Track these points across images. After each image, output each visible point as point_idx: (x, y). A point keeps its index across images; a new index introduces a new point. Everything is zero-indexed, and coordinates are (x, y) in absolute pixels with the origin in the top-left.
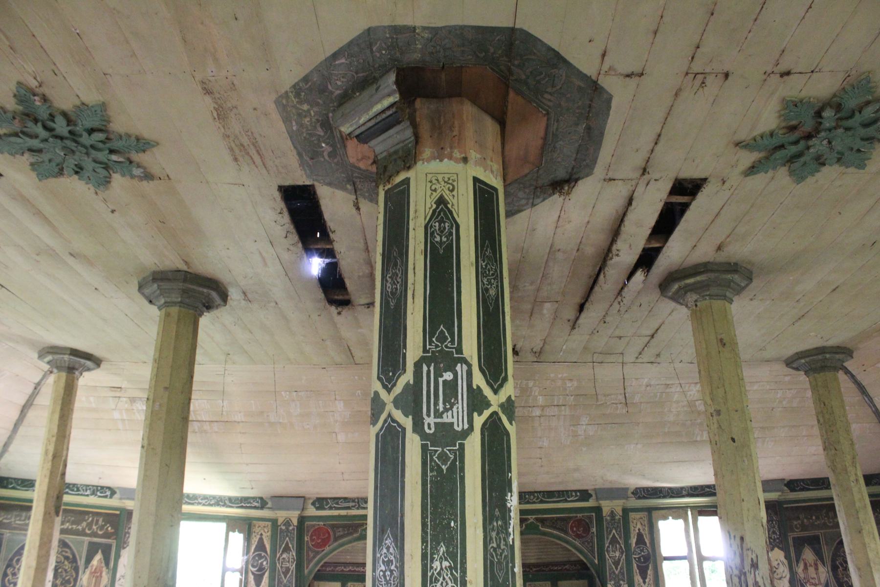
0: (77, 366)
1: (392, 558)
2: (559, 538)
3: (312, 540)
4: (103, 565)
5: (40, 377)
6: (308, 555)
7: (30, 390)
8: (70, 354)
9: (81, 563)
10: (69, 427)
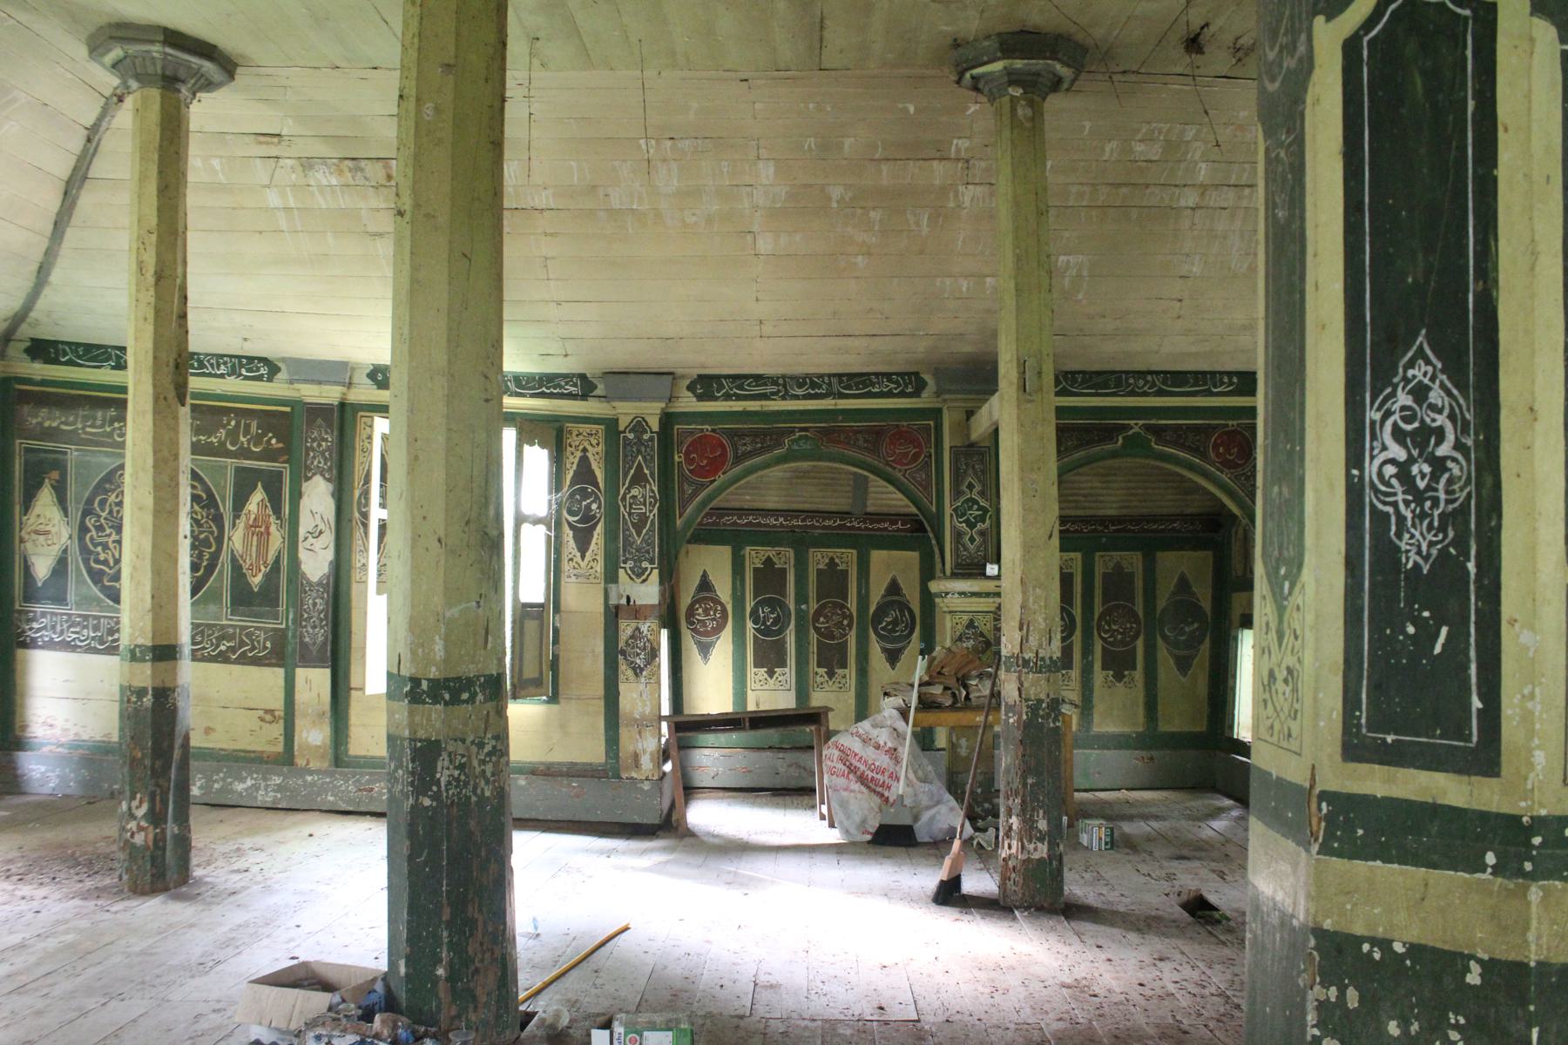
0: (182, 73)
1: (1441, 420)
2: (1191, 467)
3: (690, 461)
4: (269, 511)
5: (97, 111)
6: (682, 491)
7: (77, 144)
8: (166, 42)
9: (226, 508)
10: (181, 214)
